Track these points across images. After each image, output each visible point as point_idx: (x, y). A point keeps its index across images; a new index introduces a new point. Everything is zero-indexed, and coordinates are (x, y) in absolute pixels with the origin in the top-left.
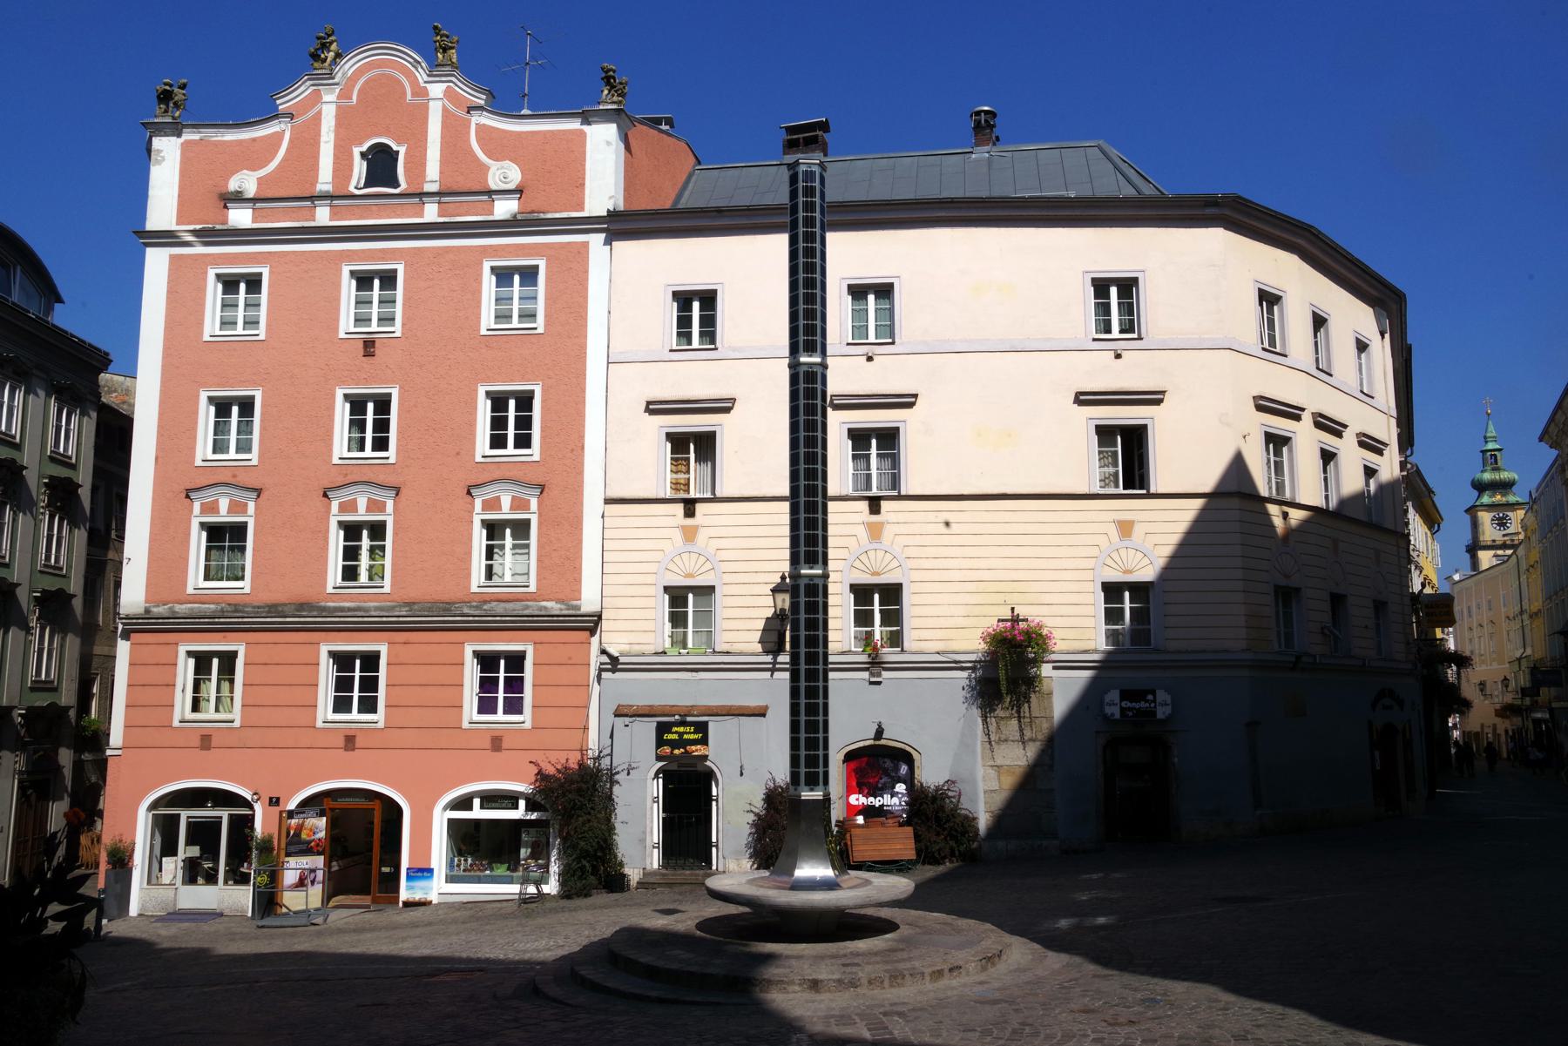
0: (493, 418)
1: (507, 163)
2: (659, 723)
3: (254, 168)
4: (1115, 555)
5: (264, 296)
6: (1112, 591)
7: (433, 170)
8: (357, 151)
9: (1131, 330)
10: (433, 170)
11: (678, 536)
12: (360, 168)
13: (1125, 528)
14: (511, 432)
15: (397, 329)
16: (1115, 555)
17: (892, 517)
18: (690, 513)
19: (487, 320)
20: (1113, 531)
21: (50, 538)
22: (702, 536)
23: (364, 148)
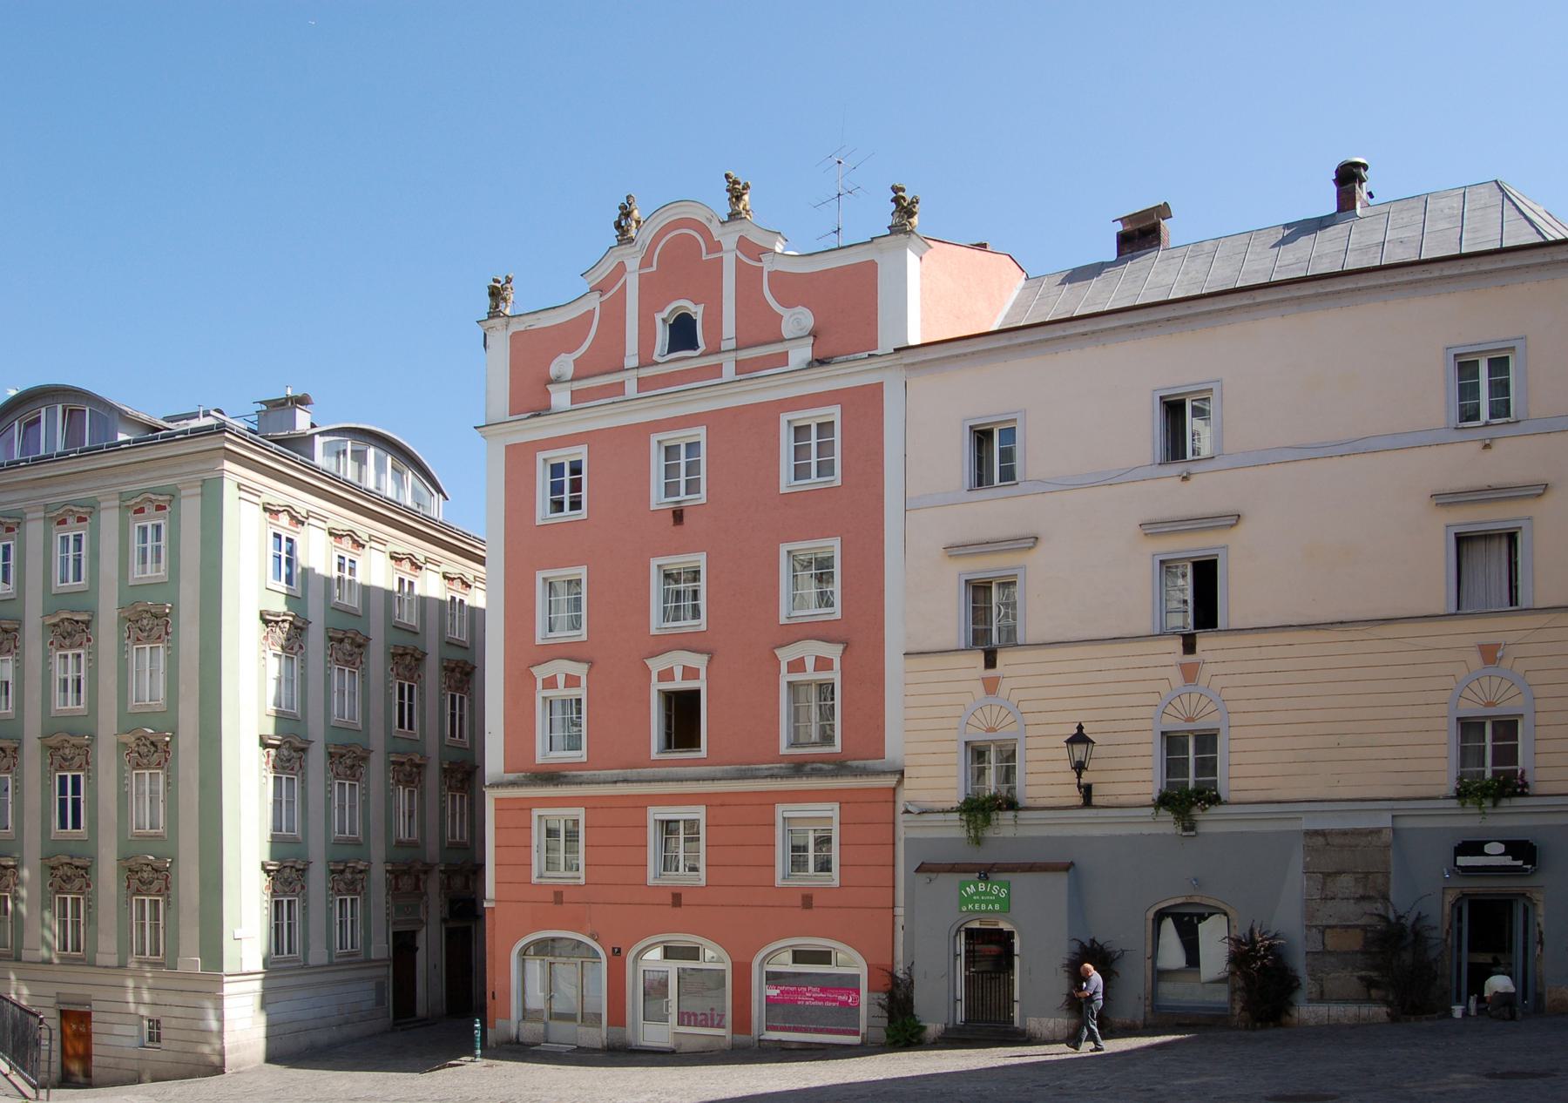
0: (1214, 772)
1: (800, 309)
2: (510, 449)
3: (570, 351)
4: (1475, 686)
5: (836, 587)
6: (1469, 727)
7: (729, 328)
8: (659, 318)
9: (667, 448)
10: (729, 328)
11: (979, 688)
12: (662, 336)
13: (1489, 654)
14: (567, 478)
15: (702, 497)
16: (1475, 686)
17: (1208, 656)
18: (990, 662)
19: (786, 481)
20: (1475, 660)
21: (453, 715)
22: (1004, 688)
23: (665, 314)
